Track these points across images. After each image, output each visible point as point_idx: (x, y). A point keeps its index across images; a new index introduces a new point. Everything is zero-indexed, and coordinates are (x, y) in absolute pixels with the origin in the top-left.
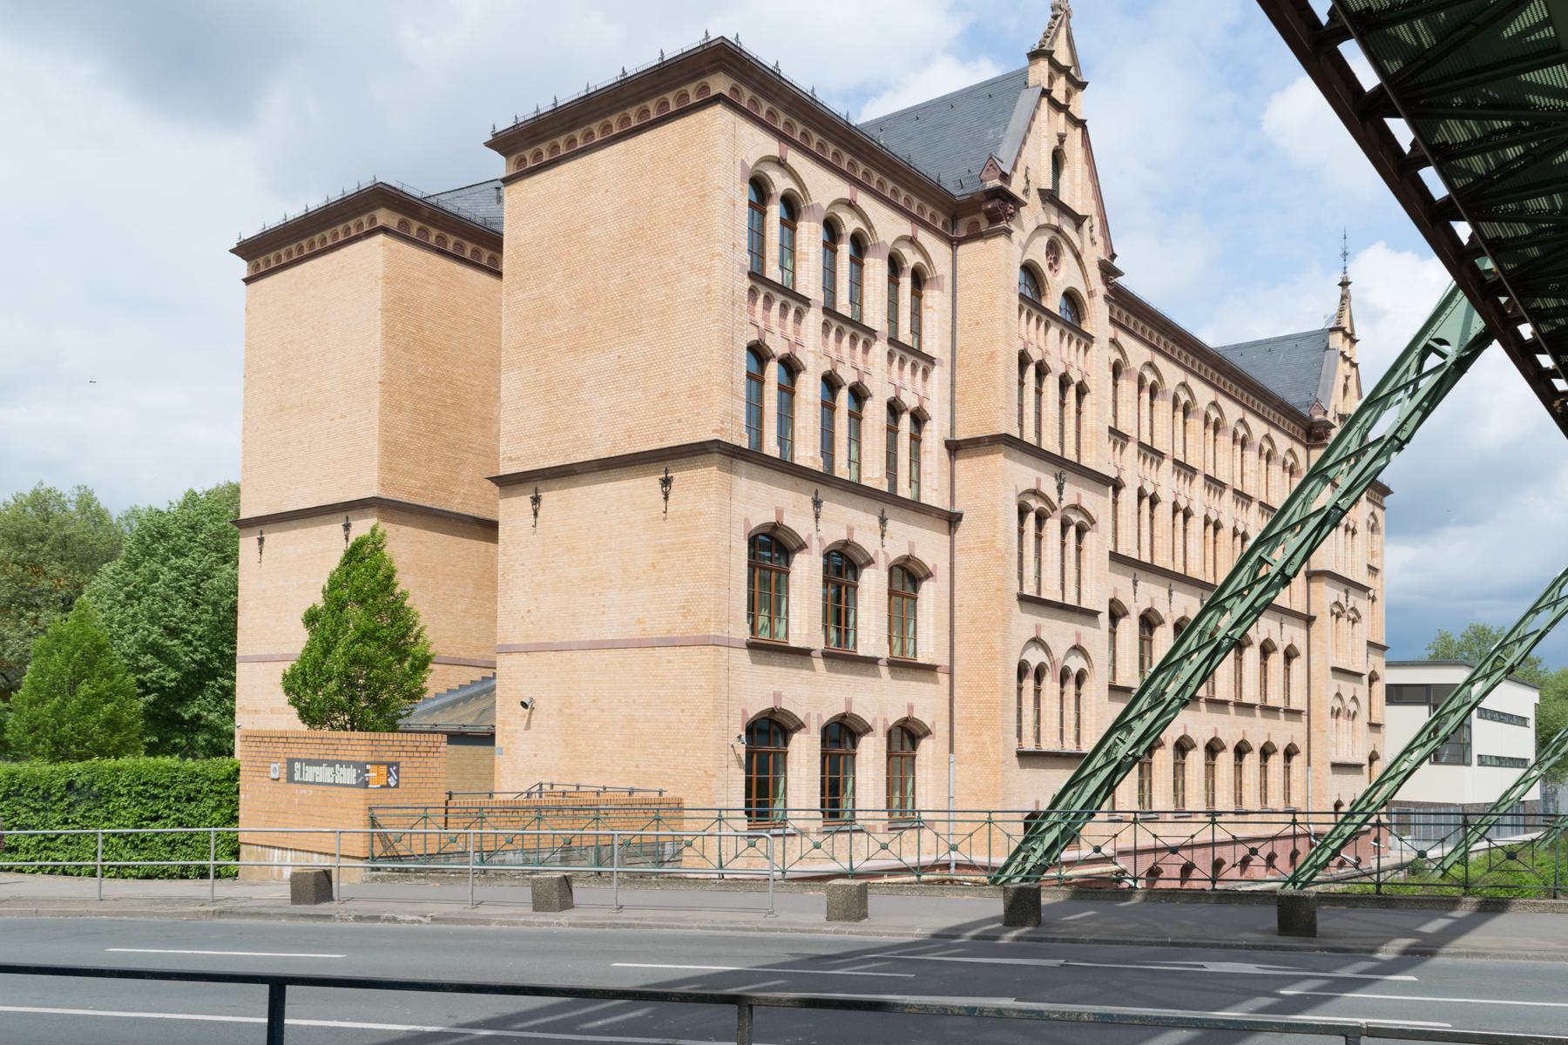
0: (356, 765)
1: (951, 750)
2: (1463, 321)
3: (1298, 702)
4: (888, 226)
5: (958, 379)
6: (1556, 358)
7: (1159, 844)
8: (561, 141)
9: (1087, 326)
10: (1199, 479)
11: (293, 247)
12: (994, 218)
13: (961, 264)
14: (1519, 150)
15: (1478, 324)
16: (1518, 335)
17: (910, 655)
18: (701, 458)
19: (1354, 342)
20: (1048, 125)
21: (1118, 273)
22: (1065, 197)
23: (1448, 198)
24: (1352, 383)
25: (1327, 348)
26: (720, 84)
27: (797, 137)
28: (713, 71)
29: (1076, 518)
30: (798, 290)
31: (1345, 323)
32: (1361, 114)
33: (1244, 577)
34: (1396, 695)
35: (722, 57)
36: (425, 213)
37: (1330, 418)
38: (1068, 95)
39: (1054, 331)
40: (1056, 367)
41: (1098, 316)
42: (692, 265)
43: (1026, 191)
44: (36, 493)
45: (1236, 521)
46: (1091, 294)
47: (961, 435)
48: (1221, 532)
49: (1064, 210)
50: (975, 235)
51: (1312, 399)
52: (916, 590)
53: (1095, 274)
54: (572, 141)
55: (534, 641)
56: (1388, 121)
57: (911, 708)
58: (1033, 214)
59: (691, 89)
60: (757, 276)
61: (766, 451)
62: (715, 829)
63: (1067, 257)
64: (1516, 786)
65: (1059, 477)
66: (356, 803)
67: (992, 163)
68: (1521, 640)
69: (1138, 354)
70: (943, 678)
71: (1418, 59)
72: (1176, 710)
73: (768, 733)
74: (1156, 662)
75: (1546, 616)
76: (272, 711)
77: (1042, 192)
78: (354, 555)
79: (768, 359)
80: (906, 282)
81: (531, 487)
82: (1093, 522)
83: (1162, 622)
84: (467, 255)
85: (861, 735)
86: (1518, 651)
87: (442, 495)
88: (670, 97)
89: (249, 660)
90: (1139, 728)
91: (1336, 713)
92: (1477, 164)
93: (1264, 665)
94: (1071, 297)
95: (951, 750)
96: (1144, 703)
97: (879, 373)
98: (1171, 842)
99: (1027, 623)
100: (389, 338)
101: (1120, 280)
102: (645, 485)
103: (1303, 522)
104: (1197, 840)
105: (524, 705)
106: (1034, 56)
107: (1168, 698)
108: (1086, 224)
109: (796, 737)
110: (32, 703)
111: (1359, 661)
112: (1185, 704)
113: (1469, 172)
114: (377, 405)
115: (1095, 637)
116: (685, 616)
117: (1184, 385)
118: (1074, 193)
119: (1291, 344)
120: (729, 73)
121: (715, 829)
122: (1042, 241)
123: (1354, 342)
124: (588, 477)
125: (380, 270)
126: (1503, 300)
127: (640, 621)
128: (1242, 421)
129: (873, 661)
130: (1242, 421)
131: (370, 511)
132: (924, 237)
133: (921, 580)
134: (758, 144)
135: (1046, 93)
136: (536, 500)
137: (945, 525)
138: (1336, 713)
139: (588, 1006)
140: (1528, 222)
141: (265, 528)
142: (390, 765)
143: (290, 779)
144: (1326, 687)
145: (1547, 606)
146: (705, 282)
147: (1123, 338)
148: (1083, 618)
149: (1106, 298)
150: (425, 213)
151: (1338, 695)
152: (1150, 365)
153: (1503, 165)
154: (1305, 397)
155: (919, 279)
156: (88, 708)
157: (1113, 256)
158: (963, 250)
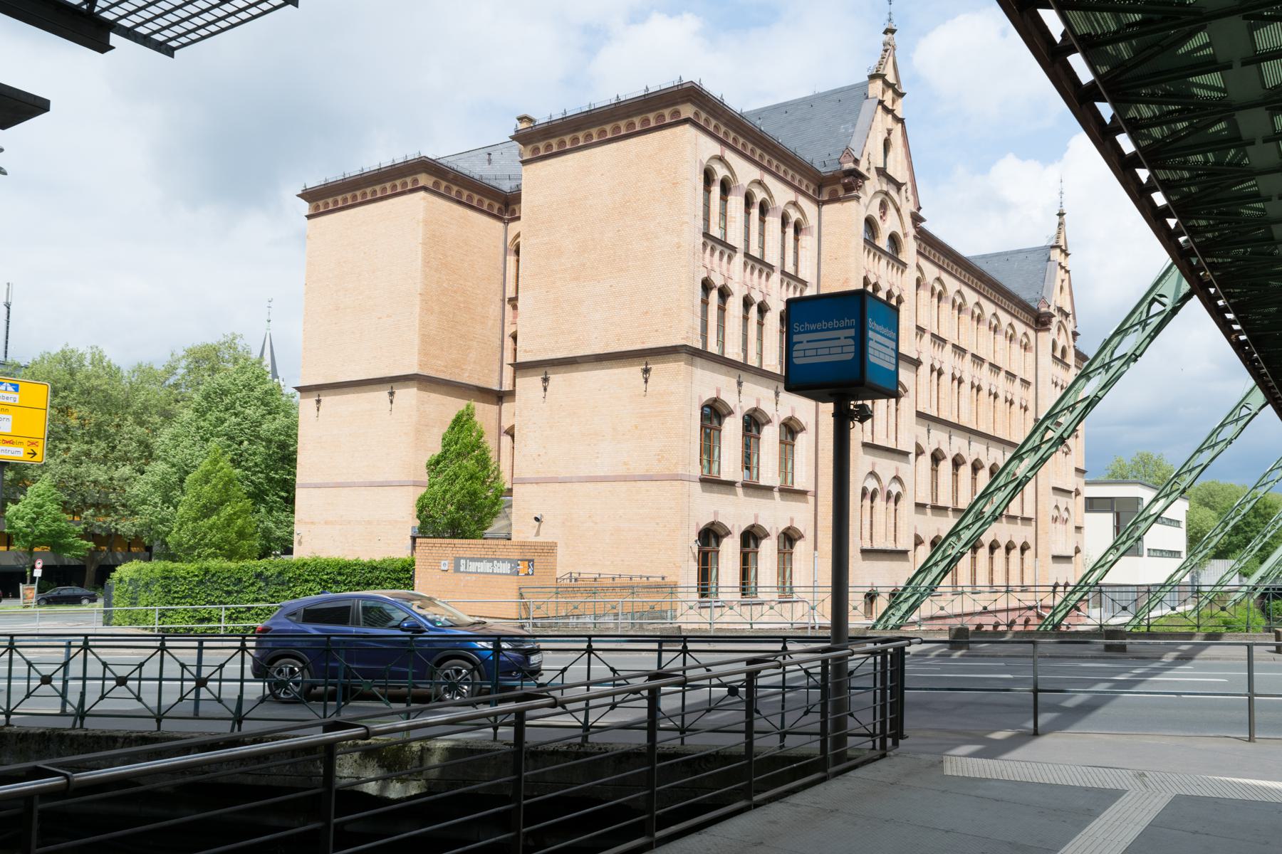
0: (510, 561)
1: (816, 549)
2: (1176, 284)
3: (1029, 513)
4: (782, 195)
6: (1236, 315)
7: (1022, 605)
8: (567, 139)
9: (902, 257)
10: (968, 357)
11: (349, 195)
12: (849, 188)
14: (1185, 124)
15: (1186, 287)
16: (1137, 177)
17: (754, 479)
19: (1067, 255)
20: (883, 122)
21: (922, 220)
22: (890, 171)
23: (1093, 82)
24: (1066, 284)
25: (1049, 260)
26: (687, 111)
27: (730, 141)
28: (683, 102)
30: (800, 276)
31: (1062, 243)
32: (1122, 167)
33: (1036, 440)
34: (1093, 505)
35: (691, 94)
36: (451, 176)
37: (1051, 310)
38: (894, 102)
39: (884, 262)
41: (910, 249)
43: (868, 169)
44: (63, 351)
45: (954, 368)
46: (905, 235)
48: (942, 377)
49: (891, 180)
50: (834, 199)
51: (1038, 297)
52: (793, 439)
56: (1041, 11)
57: (792, 520)
58: (873, 184)
59: (667, 112)
60: (706, 235)
61: (709, 350)
63: (891, 211)
64: (1178, 571)
66: (513, 583)
67: (847, 152)
68: (1190, 471)
69: (931, 272)
70: (811, 499)
71: (1120, 67)
72: (990, 523)
73: (710, 535)
74: (979, 492)
75: (1207, 455)
76: (326, 523)
77: (878, 169)
80: (755, 212)
81: (542, 370)
83: (944, 458)
84: (475, 204)
85: (762, 538)
86: (1188, 479)
87: (457, 371)
88: (651, 116)
90: (966, 535)
91: (1055, 520)
92: (1156, 132)
93: (955, 474)
94: (894, 239)
95: (816, 549)
96: (969, 519)
100: (427, 263)
101: (923, 225)
103: (1074, 406)
105: (537, 519)
106: (873, 77)
107: (986, 515)
108: (903, 188)
109: (725, 541)
111: (1071, 482)
112: (995, 519)
113: (1150, 136)
114: (417, 309)
115: (905, 469)
116: (659, 461)
117: (938, 279)
118: (897, 169)
119: (1022, 256)
120: (693, 103)
122: (877, 201)
123: (1067, 255)
124: (586, 366)
126: (1212, 290)
127: (625, 464)
128: (977, 304)
129: (770, 489)
130: (977, 304)
131: (411, 383)
132: (803, 202)
133: (797, 432)
135: (881, 102)
136: (546, 380)
138: (1055, 520)
139: (477, 739)
140: (1189, 169)
141: (321, 393)
142: (529, 561)
143: (457, 569)
144: (1049, 501)
145: (1208, 448)
146: (676, 240)
147: (923, 263)
148: (900, 457)
149: (915, 237)
151: (1057, 507)
152: (938, 279)
153: (1174, 133)
154: (1033, 295)
155: (798, 229)
157: (919, 208)
158: (825, 208)
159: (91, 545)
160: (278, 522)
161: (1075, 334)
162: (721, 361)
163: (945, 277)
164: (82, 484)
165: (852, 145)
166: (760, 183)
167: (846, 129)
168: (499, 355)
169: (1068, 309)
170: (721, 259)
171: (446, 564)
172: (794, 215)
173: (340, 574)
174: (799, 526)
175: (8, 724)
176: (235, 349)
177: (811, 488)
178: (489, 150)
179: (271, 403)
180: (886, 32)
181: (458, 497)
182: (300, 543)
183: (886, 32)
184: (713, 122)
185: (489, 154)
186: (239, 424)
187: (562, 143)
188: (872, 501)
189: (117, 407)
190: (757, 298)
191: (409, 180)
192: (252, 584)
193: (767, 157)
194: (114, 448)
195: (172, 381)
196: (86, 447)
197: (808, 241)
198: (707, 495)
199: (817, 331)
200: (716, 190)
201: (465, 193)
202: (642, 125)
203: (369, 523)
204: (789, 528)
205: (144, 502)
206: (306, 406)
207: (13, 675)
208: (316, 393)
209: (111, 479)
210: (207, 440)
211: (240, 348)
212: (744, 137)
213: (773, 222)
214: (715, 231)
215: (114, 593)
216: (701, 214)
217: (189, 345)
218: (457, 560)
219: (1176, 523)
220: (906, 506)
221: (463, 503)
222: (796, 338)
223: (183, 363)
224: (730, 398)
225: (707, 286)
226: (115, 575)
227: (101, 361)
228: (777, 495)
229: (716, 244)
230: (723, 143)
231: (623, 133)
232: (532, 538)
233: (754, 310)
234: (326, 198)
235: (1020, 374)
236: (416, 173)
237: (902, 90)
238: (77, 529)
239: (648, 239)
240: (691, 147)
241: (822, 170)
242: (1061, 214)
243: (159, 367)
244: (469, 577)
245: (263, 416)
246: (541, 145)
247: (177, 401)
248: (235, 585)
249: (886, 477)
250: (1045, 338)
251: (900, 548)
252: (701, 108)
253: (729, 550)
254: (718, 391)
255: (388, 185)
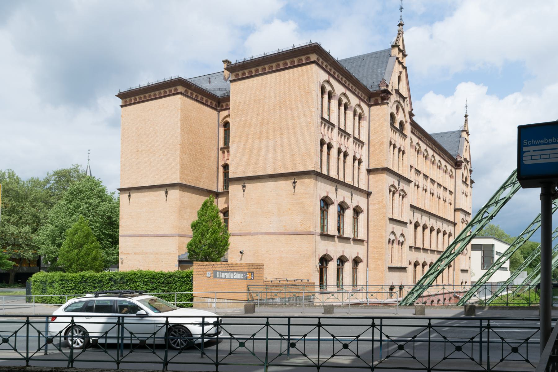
0: (242, 272)
4: (354, 101)
5: (370, 149)
8: (253, 70)
11: (142, 96)
12: (384, 99)
13: (371, 112)
18: (308, 176)
19: (468, 135)
21: (413, 115)
22: (400, 91)
25: (461, 137)
26: (314, 57)
28: (312, 53)
29: (402, 193)
31: (466, 129)
35: (316, 49)
36: (193, 88)
37: (462, 159)
39: (397, 134)
40: (398, 146)
41: (408, 129)
42: (304, 115)
43: (392, 90)
46: (406, 122)
47: (371, 167)
49: (401, 96)
50: (376, 104)
53: (407, 115)
54: (258, 70)
55: (243, 232)
57: (358, 253)
58: (394, 98)
59: (303, 58)
60: (322, 118)
62: (380, 291)
64: (484, 276)
65: (399, 181)
66: (244, 284)
67: (383, 81)
69: (416, 140)
70: (365, 244)
73: (324, 260)
76: (135, 254)
77: (396, 90)
78: (205, 205)
79: (324, 144)
82: (406, 194)
84: (204, 102)
87: (197, 182)
89: (123, 236)
94: (401, 124)
95: (367, 266)
97: (350, 147)
98: (432, 293)
99: (391, 227)
100: (182, 130)
101: (414, 118)
102: (287, 184)
104: (439, 293)
105: (241, 252)
106: (393, 46)
110: (67, 252)
116: (301, 225)
119: (448, 135)
120: (317, 54)
121: (380, 291)
122: (395, 106)
123: (468, 135)
124: (264, 180)
125: (179, 107)
127: (284, 226)
131: (176, 187)
132: (363, 105)
133: (360, 213)
134: (324, 76)
135: (397, 58)
137: (366, 195)
141: (131, 191)
142: (252, 273)
148: (403, 225)
150: (193, 88)
156: (88, 254)
157: (412, 110)
158: (372, 108)
159: (14, 263)
160: (108, 254)
161: (471, 171)
162: (327, 178)
163: (421, 143)
164: (6, 235)
165: (385, 78)
166: (344, 94)
167: (381, 71)
168: (216, 175)
169: (468, 159)
170: (328, 130)
171: (209, 274)
172: (359, 111)
173: (153, 279)
174: (361, 256)
175: (28, 365)
176: (78, 172)
177: (366, 239)
178: (209, 76)
179: (101, 195)
180: (399, 25)
181: (209, 241)
182: (122, 263)
183: (399, 25)
184: (325, 64)
185: (209, 78)
186: (87, 208)
187: (251, 72)
188: (392, 245)
189: (22, 198)
190: (343, 149)
191: (173, 89)
192: (108, 283)
193: (348, 82)
194: (21, 218)
195: (48, 186)
196: (7, 218)
197: (364, 123)
198: (323, 241)
199: (540, 144)
200: (326, 97)
201: (200, 96)
202: (291, 64)
203: (157, 254)
204: (342, 256)
205: (43, 244)
206: (124, 197)
207: (29, 335)
208: (128, 192)
209: (20, 233)
210: (73, 214)
211: (80, 172)
212: (338, 72)
213: (350, 113)
214: (326, 116)
215: (32, 287)
216: (320, 108)
217: (55, 170)
218: (215, 272)
219: (505, 269)
220: (406, 247)
221: (209, 243)
222: (525, 149)
223: (53, 178)
224: (332, 196)
225: (322, 143)
226: (32, 279)
227: (13, 176)
228: (352, 242)
229: (326, 122)
230: (329, 74)
231: (281, 67)
232: (239, 262)
233: (342, 155)
234: (130, 97)
235: (449, 188)
236: (177, 86)
237: (406, 53)
238: (7, 256)
239: (294, 120)
240: (315, 75)
241: (371, 90)
242: (466, 116)
243: (42, 180)
244: (221, 280)
245: (99, 203)
246: (240, 73)
247: (51, 196)
248: (98, 283)
249: (398, 234)
250: (459, 172)
251: (403, 266)
252: (320, 56)
253: (332, 267)
254: (327, 193)
255: (162, 91)
